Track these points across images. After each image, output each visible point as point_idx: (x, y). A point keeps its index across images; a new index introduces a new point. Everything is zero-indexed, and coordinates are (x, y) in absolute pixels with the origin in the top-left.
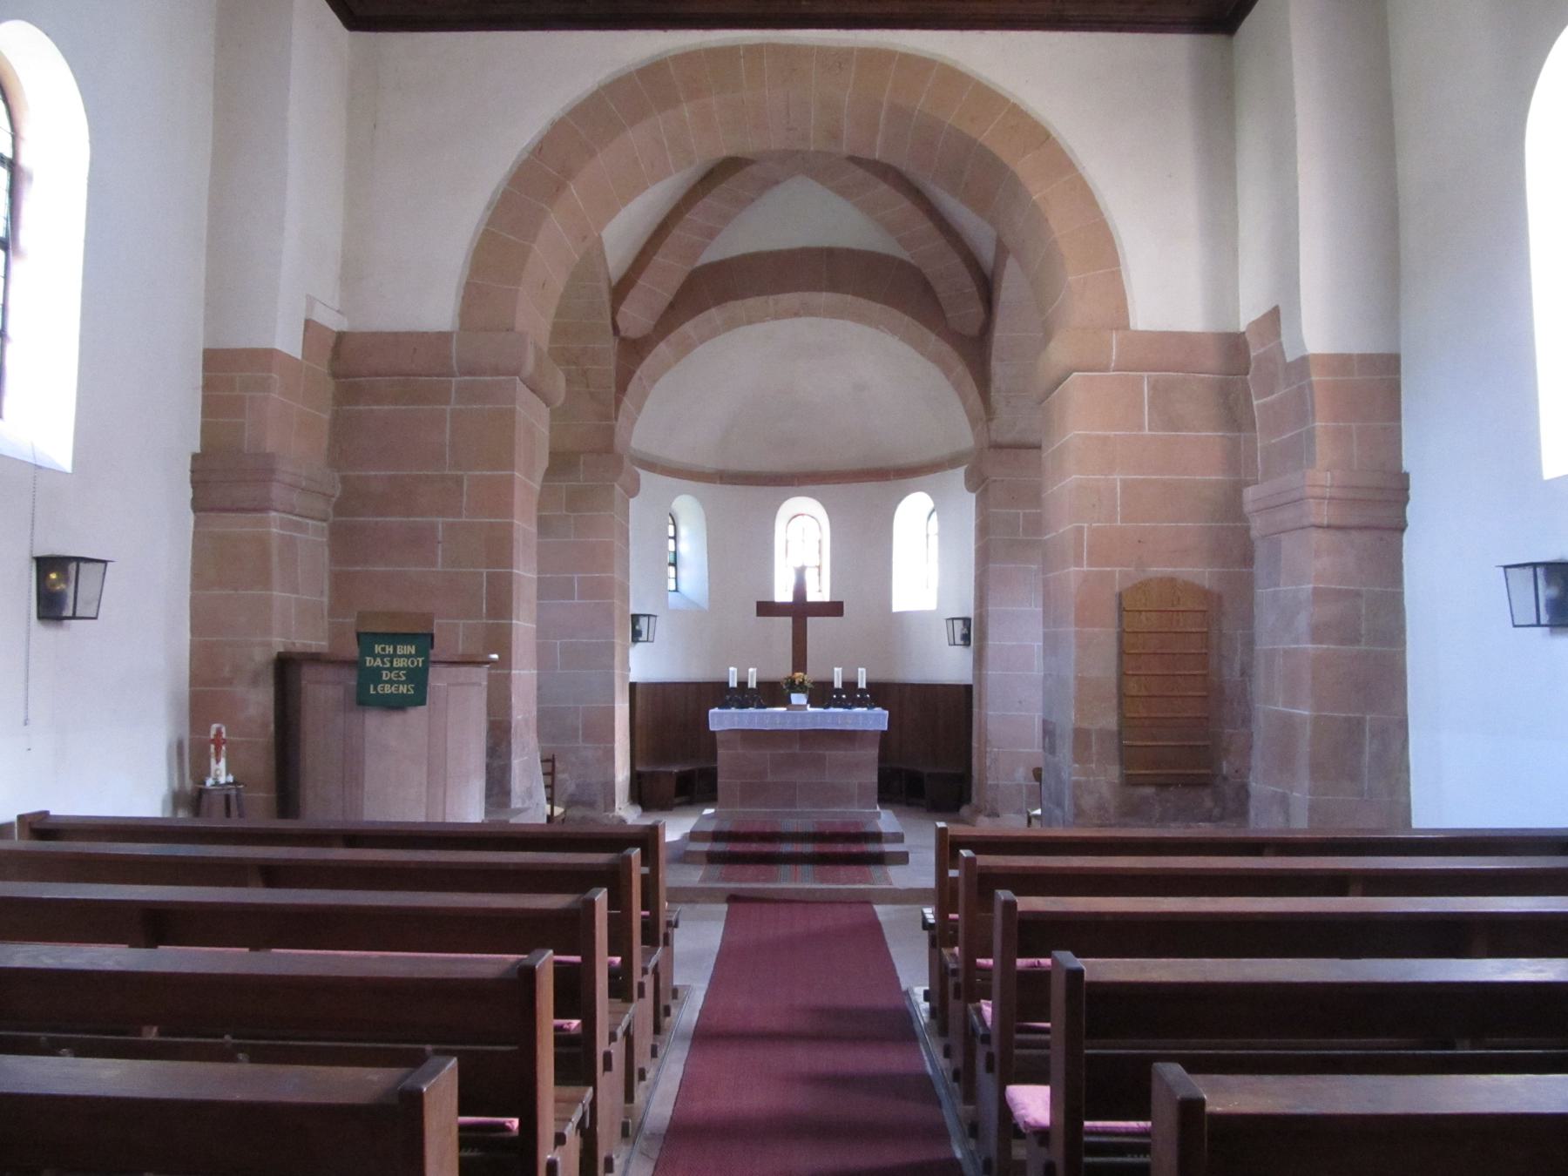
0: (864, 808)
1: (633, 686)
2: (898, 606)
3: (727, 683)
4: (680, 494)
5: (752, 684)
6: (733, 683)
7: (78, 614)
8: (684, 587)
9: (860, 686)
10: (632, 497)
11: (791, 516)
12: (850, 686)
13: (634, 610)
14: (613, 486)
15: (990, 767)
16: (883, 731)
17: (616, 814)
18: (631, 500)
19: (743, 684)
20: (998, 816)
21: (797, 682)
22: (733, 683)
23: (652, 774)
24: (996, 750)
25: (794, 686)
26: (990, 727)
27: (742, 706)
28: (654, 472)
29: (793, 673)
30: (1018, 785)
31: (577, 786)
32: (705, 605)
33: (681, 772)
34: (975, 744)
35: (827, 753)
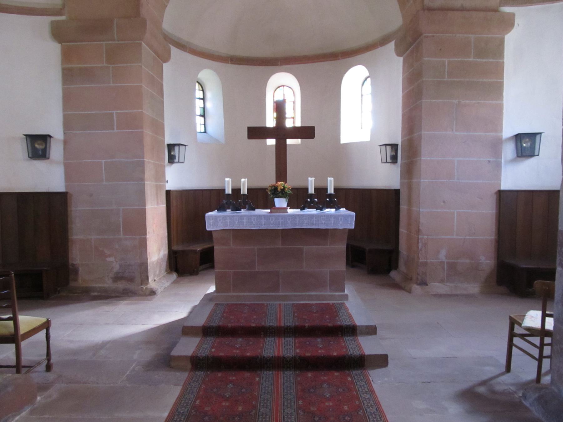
0: (336, 291)
1: (168, 192)
2: (345, 139)
3: (224, 190)
4: (205, 68)
5: (244, 191)
6: (229, 191)
7: (180, 161)
8: (209, 130)
9: (329, 192)
10: (165, 61)
11: (276, 87)
12: (321, 191)
13: (168, 140)
14: (141, 44)
15: (421, 250)
16: (350, 230)
17: (148, 286)
18: (164, 65)
19: (236, 191)
20: (427, 285)
21: (279, 190)
22: (229, 191)
23: (183, 252)
24: (425, 237)
25: (277, 192)
26: (422, 220)
27: (237, 208)
28: (185, 51)
29: (276, 183)
30: (441, 262)
31: (121, 266)
32: (222, 140)
33: (202, 250)
34: (403, 230)
35: (305, 248)
